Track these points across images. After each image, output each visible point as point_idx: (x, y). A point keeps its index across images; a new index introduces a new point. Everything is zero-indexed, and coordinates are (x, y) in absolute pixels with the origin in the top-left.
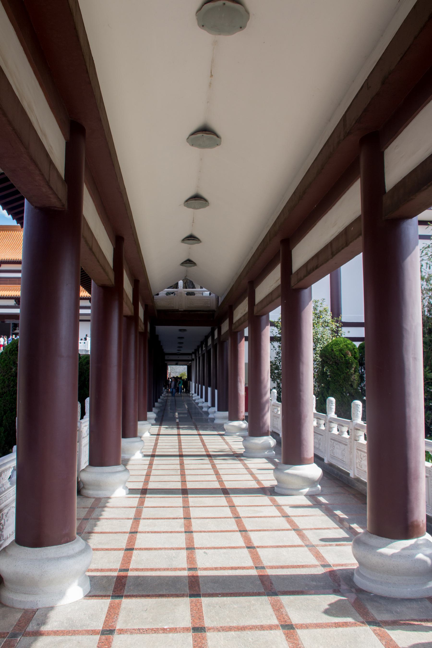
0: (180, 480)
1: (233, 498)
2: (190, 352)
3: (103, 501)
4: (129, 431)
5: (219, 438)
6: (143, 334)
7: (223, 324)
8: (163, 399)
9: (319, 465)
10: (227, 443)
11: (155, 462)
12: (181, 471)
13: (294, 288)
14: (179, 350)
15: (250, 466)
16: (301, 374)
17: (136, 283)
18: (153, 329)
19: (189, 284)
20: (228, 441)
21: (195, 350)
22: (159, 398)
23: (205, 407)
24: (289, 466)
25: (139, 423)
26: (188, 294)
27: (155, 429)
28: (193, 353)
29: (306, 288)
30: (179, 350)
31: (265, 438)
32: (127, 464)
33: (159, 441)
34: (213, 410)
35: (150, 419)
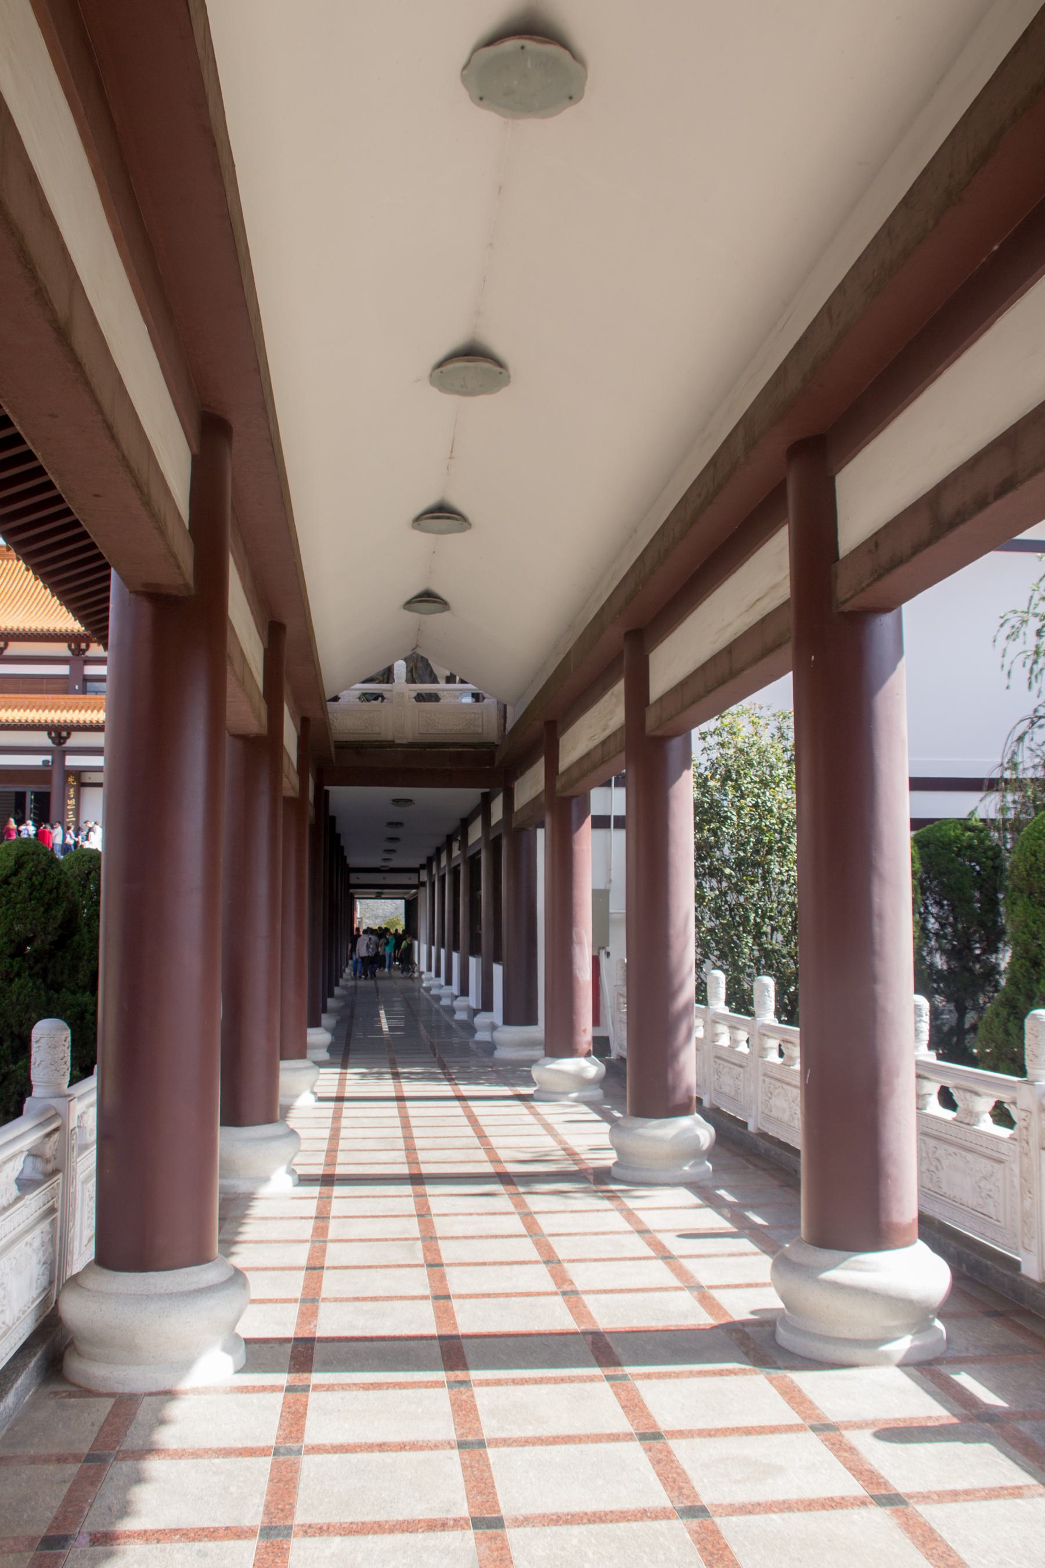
0: (428, 1292)
1: (639, 1384)
2: (416, 864)
3: (143, 1413)
4: (247, 1102)
5: (519, 1107)
6: (295, 804)
7: (520, 780)
8: (358, 1001)
9: (937, 1247)
10: (549, 1128)
11: (337, 1207)
12: (427, 1249)
13: (847, 607)
14: (385, 860)
15: (651, 1220)
16: (876, 921)
17: (274, 632)
18: (322, 799)
19: (420, 669)
20: (550, 1119)
21: (430, 860)
22: (337, 985)
23: (462, 1009)
24: (838, 1254)
25: (283, 1064)
26: (420, 698)
27: (328, 1079)
28: (422, 867)
29: (888, 610)
30: (385, 860)
31: (685, 1122)
32: (245, 1216)
33: (344, 1122)
34: (488, 1021)
35: (316, 1047)
